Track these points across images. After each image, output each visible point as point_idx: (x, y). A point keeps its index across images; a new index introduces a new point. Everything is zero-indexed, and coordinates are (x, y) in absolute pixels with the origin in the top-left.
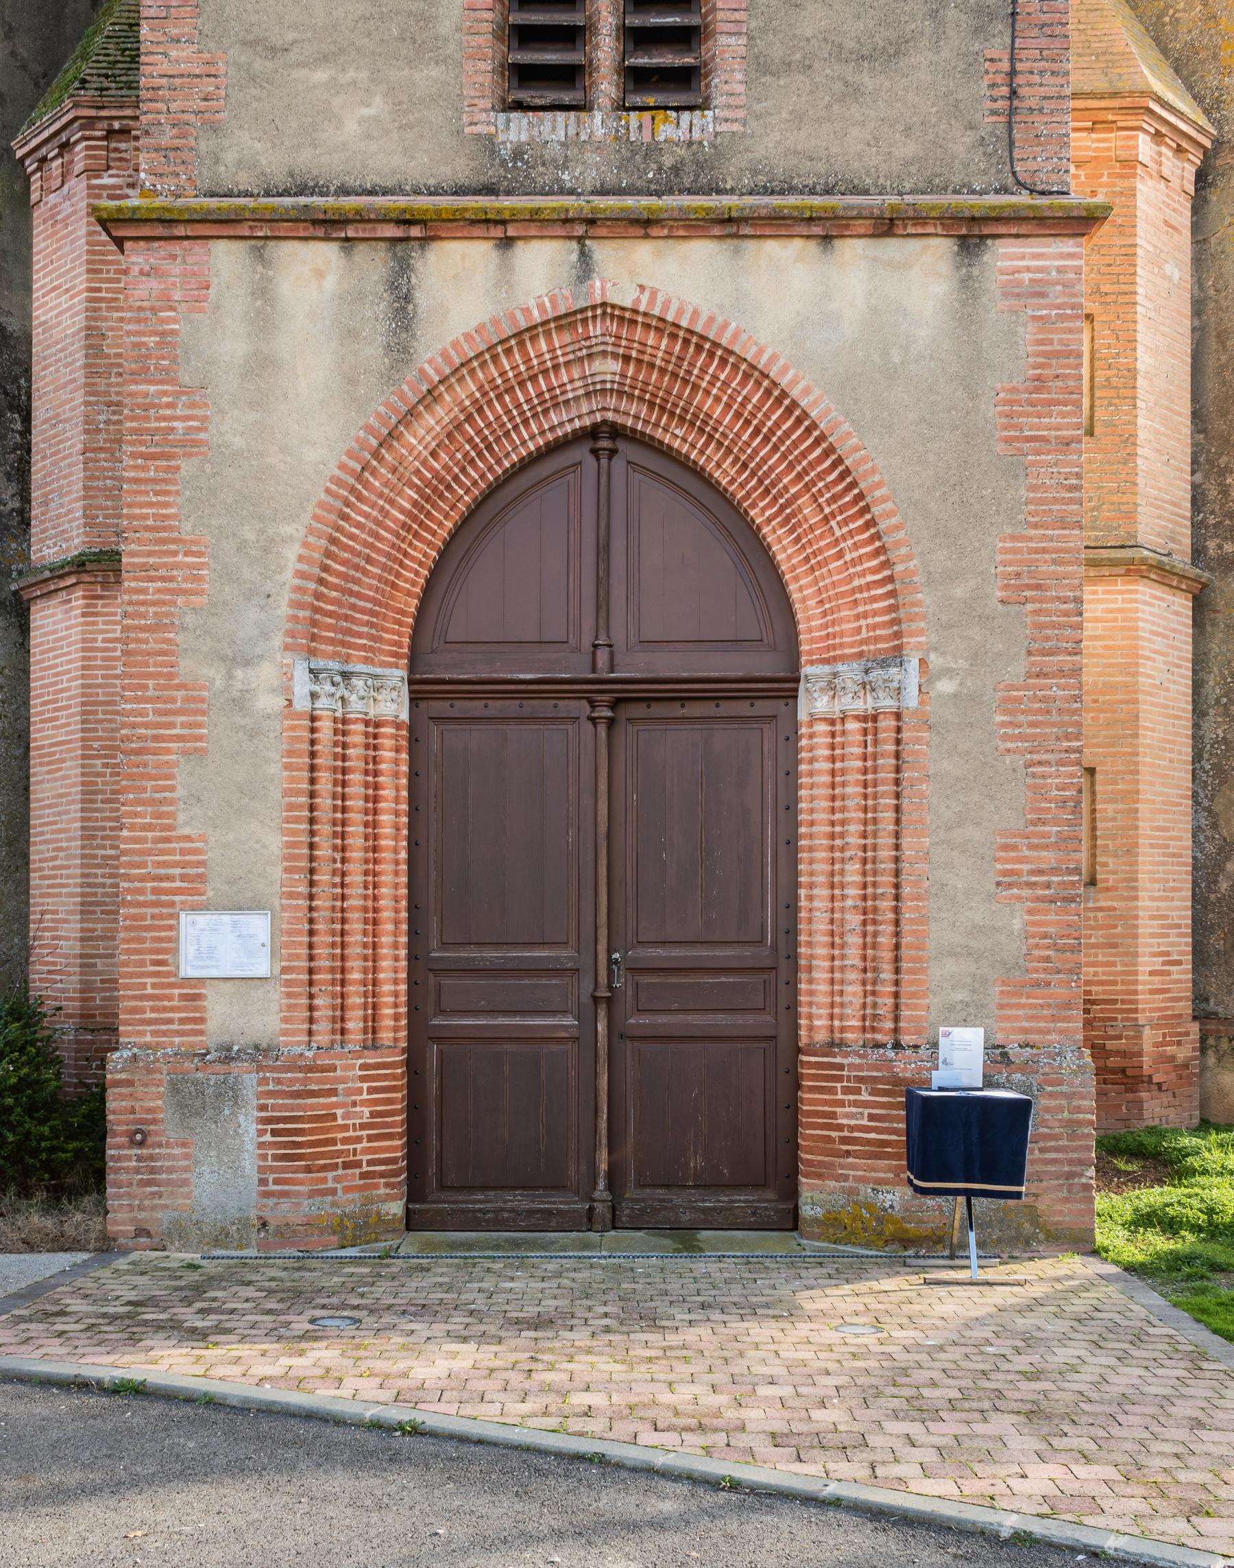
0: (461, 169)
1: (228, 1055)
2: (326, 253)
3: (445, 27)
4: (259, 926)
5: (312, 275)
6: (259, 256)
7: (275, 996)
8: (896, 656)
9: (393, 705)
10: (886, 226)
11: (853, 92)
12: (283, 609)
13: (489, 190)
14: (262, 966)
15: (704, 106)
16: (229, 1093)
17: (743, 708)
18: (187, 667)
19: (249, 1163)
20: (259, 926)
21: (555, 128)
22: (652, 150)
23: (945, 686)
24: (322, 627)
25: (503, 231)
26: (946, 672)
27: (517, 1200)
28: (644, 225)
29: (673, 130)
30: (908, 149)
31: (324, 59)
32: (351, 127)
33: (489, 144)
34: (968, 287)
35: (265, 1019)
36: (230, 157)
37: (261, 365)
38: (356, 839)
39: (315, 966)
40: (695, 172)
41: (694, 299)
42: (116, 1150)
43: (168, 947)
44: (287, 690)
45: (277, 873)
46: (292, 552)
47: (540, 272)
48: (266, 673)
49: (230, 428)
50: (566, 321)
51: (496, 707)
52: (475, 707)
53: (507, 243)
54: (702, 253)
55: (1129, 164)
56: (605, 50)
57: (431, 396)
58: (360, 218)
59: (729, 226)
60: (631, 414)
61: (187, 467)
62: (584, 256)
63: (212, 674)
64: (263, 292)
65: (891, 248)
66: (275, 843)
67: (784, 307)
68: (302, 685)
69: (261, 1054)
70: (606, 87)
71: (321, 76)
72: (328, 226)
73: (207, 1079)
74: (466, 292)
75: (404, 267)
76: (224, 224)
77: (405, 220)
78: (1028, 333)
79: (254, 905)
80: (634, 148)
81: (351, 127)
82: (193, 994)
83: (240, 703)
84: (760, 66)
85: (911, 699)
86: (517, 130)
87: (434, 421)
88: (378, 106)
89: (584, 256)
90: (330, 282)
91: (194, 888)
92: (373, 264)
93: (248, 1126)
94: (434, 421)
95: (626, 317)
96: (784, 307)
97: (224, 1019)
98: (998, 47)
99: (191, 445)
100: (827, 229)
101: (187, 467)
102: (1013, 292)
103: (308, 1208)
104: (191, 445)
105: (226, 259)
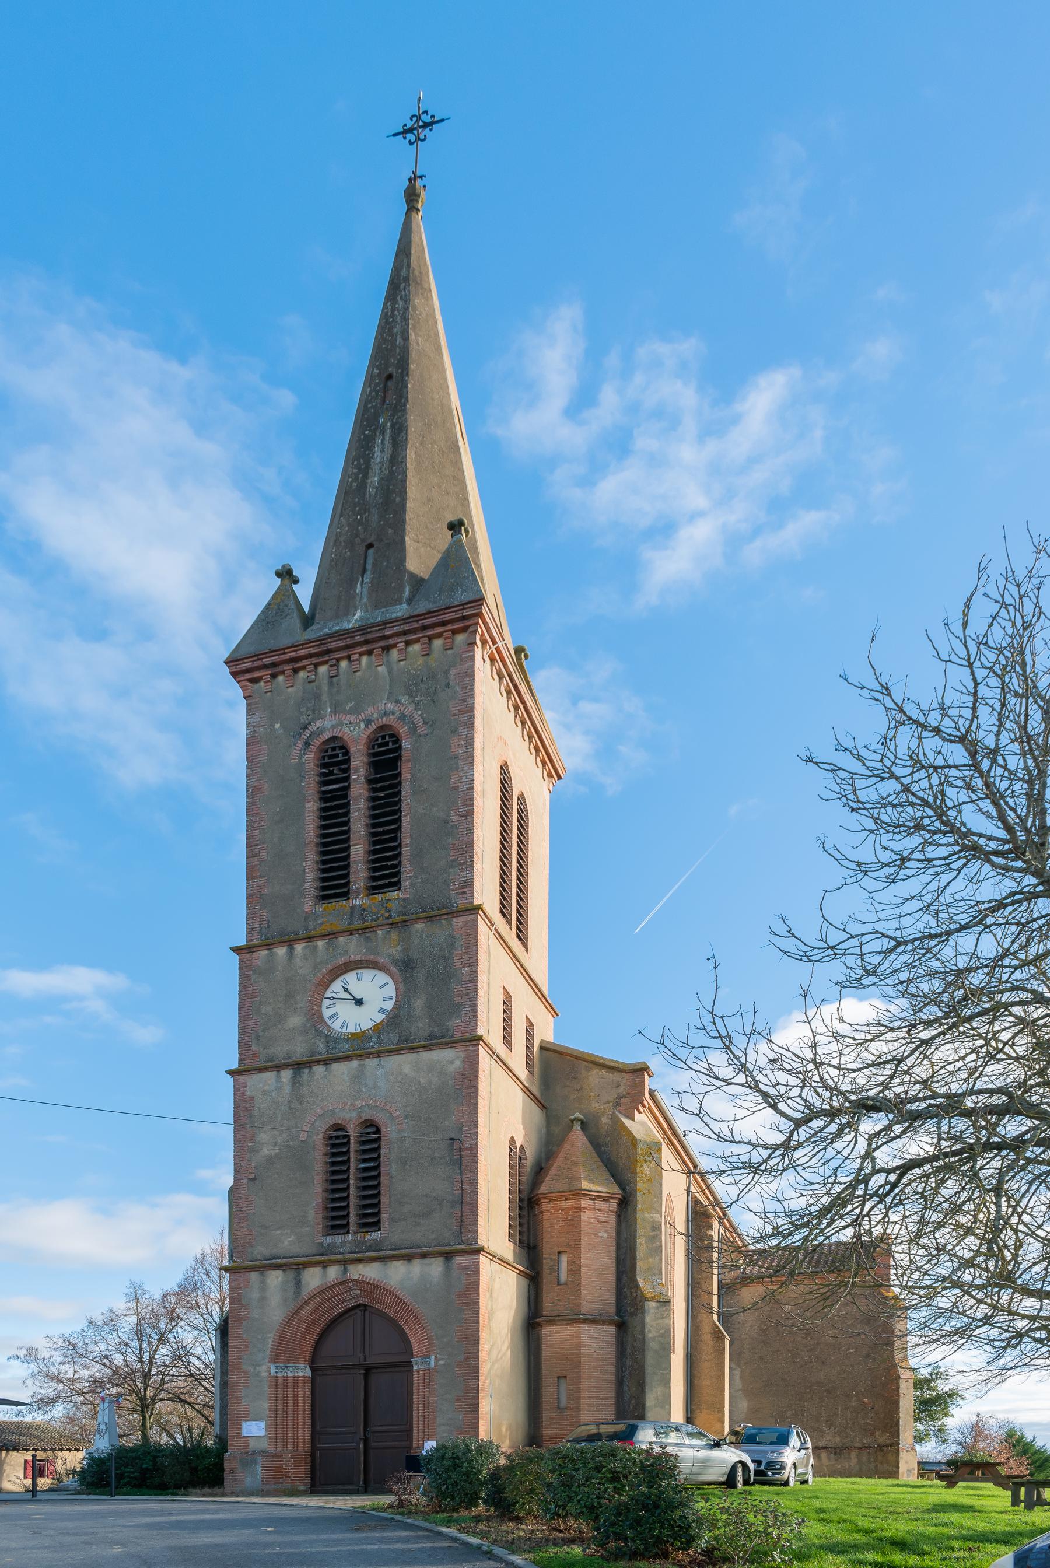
0: (314, 1251)
1: (254, 1453)
2: (279, 1273)
3: (310, 1219)
4: (262, 1424)
5: (275, 1279)
6: (262, 1275)
7: (266, 1439)
8: (429, 1357)
9: (308, 1373)
10: (424, 1256)
11: (418, 1224)
12: (268, 1353)
13: (322, 1255)
14: (263, 1433)
15: (379, 1230)
16: (254, 1462)
17: (402, 1369)
18: (244, 1367)
19: (259, 1477)
20: (262, 1424)
21: (339, 1239)
22: (365, 1242)
23: (441, 1362)
24: (279, 1356)
25: (324, 1265)
26: (442, 1359)
27: (340, 1487)
28: (359, 1261)
29: (372, 1236)
30: (433, 1236)
31: (279, 1228)
32: (286, 1243)
33: (321, 1244)
34: (448, 1269)
35: (264, 1445)
36: (256, 1252)
37: (263, 1299)
38: (290, 1402)
39: (278, 1431)
40: (377, 1246)
41: (373, 1276)
42: (226, 1475)
43: (240, 1429)
44: (269, 1372)
45: (267, 1412)
46: (270, 1341)
47: (333, 1273)
48: (264, 1367)
49: (255, 1314)
50: (341, 1283)
51: (334, 1372)
52: (329, 1372)
53: (325, 1267)
54: (376, 1265)
55: (579, 1209)
56: (353, 1219)
57: (306, 1303)
58: (286, 1265)
59: (382, 1259)
60: (366, 1302)
61: (244, 1323)
62: (345, 1268)
63: (251, 1369)
64: (263, 1283)
65: (427, 1261)
66: (266, 1406)
67: (397, 1276)
68: (273, 1370)
69: (262, 1453)
70: (352, 1229)
71: (278, 1232)
72: (278, 1267)
73: (249, 1458)
74: (313, 1279)
75: (299, 1274)
76: (253, 1268)
77: (297, 1264)
78: (464, 1278)
79: (261, 1420)
80: (359, 1242)
81: (286, 1243)
82: (246, 1439)
83: (258, 1375)
84: (392, 1220)
85: (432, 1365)
86: (329, 1240)
87: (308, 1308)
88: (293, 1238)
89: (345, 1268)
90: (280, 1279)
91: (247, 1417)
92: (291, 1275)
93: (259, 1469)
94: (308, 1308)
95: (358, 1281)
96: (397, 1276)
97: (252, 1444)
98: (458, 1210)
99: (246, 1318)
100: (409, 1258)
101: (244, 1323)
102: (461, 1269)
103: (273, 1486)
104: (246, 1318)
105: (254, 1276)
